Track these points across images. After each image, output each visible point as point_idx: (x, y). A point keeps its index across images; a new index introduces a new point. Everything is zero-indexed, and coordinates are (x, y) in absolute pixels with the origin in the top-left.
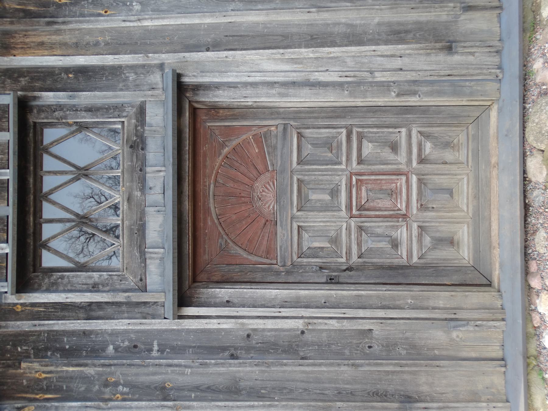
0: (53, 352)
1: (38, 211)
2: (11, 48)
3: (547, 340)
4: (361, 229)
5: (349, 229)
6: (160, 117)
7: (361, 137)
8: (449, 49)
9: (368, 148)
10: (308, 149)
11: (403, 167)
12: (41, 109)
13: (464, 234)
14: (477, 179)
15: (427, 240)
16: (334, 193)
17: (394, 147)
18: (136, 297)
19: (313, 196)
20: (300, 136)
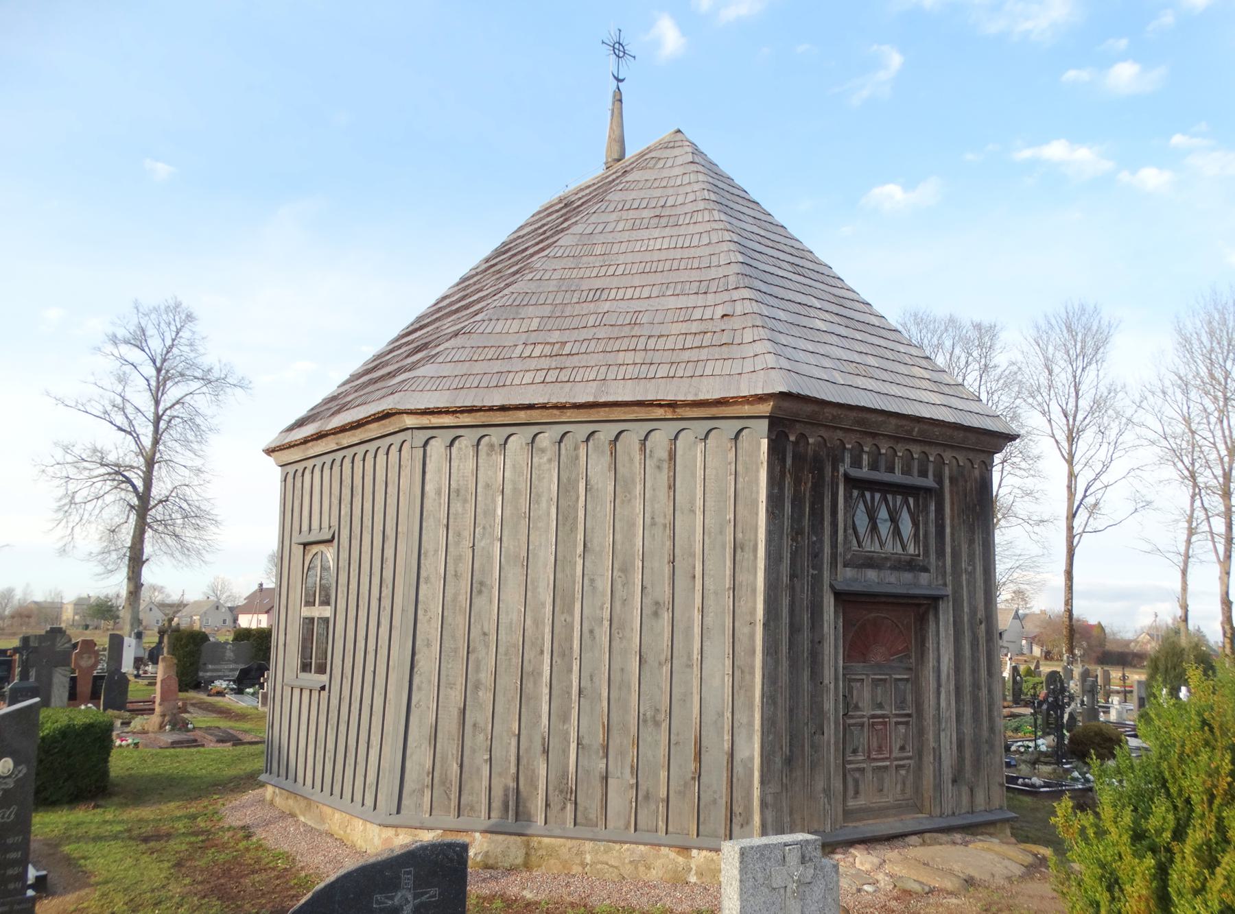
0: (1035, 696)
1: (878, 491)
2: (972, 530)
3: (1234, 509)
4: (862, 725)
5: (863, 716)
6: (924, 583)
7: (907, 723)
8: (954, 781)
9: (902, 729)
10: (901, 685)
11: (894, 755)
12: (925, 499)
13: (861, 802)
14: (888, 808)
15: (857, 775)
16: (880, 706)
17: (902, 748)
18: (840, 560)
19: (879, 690)
20: (907, 680)
